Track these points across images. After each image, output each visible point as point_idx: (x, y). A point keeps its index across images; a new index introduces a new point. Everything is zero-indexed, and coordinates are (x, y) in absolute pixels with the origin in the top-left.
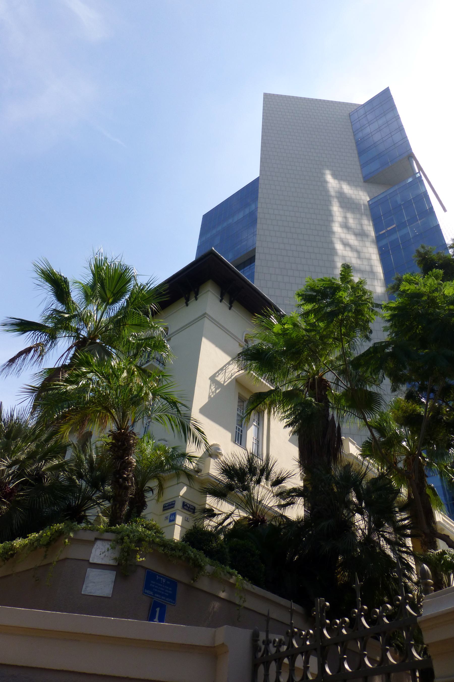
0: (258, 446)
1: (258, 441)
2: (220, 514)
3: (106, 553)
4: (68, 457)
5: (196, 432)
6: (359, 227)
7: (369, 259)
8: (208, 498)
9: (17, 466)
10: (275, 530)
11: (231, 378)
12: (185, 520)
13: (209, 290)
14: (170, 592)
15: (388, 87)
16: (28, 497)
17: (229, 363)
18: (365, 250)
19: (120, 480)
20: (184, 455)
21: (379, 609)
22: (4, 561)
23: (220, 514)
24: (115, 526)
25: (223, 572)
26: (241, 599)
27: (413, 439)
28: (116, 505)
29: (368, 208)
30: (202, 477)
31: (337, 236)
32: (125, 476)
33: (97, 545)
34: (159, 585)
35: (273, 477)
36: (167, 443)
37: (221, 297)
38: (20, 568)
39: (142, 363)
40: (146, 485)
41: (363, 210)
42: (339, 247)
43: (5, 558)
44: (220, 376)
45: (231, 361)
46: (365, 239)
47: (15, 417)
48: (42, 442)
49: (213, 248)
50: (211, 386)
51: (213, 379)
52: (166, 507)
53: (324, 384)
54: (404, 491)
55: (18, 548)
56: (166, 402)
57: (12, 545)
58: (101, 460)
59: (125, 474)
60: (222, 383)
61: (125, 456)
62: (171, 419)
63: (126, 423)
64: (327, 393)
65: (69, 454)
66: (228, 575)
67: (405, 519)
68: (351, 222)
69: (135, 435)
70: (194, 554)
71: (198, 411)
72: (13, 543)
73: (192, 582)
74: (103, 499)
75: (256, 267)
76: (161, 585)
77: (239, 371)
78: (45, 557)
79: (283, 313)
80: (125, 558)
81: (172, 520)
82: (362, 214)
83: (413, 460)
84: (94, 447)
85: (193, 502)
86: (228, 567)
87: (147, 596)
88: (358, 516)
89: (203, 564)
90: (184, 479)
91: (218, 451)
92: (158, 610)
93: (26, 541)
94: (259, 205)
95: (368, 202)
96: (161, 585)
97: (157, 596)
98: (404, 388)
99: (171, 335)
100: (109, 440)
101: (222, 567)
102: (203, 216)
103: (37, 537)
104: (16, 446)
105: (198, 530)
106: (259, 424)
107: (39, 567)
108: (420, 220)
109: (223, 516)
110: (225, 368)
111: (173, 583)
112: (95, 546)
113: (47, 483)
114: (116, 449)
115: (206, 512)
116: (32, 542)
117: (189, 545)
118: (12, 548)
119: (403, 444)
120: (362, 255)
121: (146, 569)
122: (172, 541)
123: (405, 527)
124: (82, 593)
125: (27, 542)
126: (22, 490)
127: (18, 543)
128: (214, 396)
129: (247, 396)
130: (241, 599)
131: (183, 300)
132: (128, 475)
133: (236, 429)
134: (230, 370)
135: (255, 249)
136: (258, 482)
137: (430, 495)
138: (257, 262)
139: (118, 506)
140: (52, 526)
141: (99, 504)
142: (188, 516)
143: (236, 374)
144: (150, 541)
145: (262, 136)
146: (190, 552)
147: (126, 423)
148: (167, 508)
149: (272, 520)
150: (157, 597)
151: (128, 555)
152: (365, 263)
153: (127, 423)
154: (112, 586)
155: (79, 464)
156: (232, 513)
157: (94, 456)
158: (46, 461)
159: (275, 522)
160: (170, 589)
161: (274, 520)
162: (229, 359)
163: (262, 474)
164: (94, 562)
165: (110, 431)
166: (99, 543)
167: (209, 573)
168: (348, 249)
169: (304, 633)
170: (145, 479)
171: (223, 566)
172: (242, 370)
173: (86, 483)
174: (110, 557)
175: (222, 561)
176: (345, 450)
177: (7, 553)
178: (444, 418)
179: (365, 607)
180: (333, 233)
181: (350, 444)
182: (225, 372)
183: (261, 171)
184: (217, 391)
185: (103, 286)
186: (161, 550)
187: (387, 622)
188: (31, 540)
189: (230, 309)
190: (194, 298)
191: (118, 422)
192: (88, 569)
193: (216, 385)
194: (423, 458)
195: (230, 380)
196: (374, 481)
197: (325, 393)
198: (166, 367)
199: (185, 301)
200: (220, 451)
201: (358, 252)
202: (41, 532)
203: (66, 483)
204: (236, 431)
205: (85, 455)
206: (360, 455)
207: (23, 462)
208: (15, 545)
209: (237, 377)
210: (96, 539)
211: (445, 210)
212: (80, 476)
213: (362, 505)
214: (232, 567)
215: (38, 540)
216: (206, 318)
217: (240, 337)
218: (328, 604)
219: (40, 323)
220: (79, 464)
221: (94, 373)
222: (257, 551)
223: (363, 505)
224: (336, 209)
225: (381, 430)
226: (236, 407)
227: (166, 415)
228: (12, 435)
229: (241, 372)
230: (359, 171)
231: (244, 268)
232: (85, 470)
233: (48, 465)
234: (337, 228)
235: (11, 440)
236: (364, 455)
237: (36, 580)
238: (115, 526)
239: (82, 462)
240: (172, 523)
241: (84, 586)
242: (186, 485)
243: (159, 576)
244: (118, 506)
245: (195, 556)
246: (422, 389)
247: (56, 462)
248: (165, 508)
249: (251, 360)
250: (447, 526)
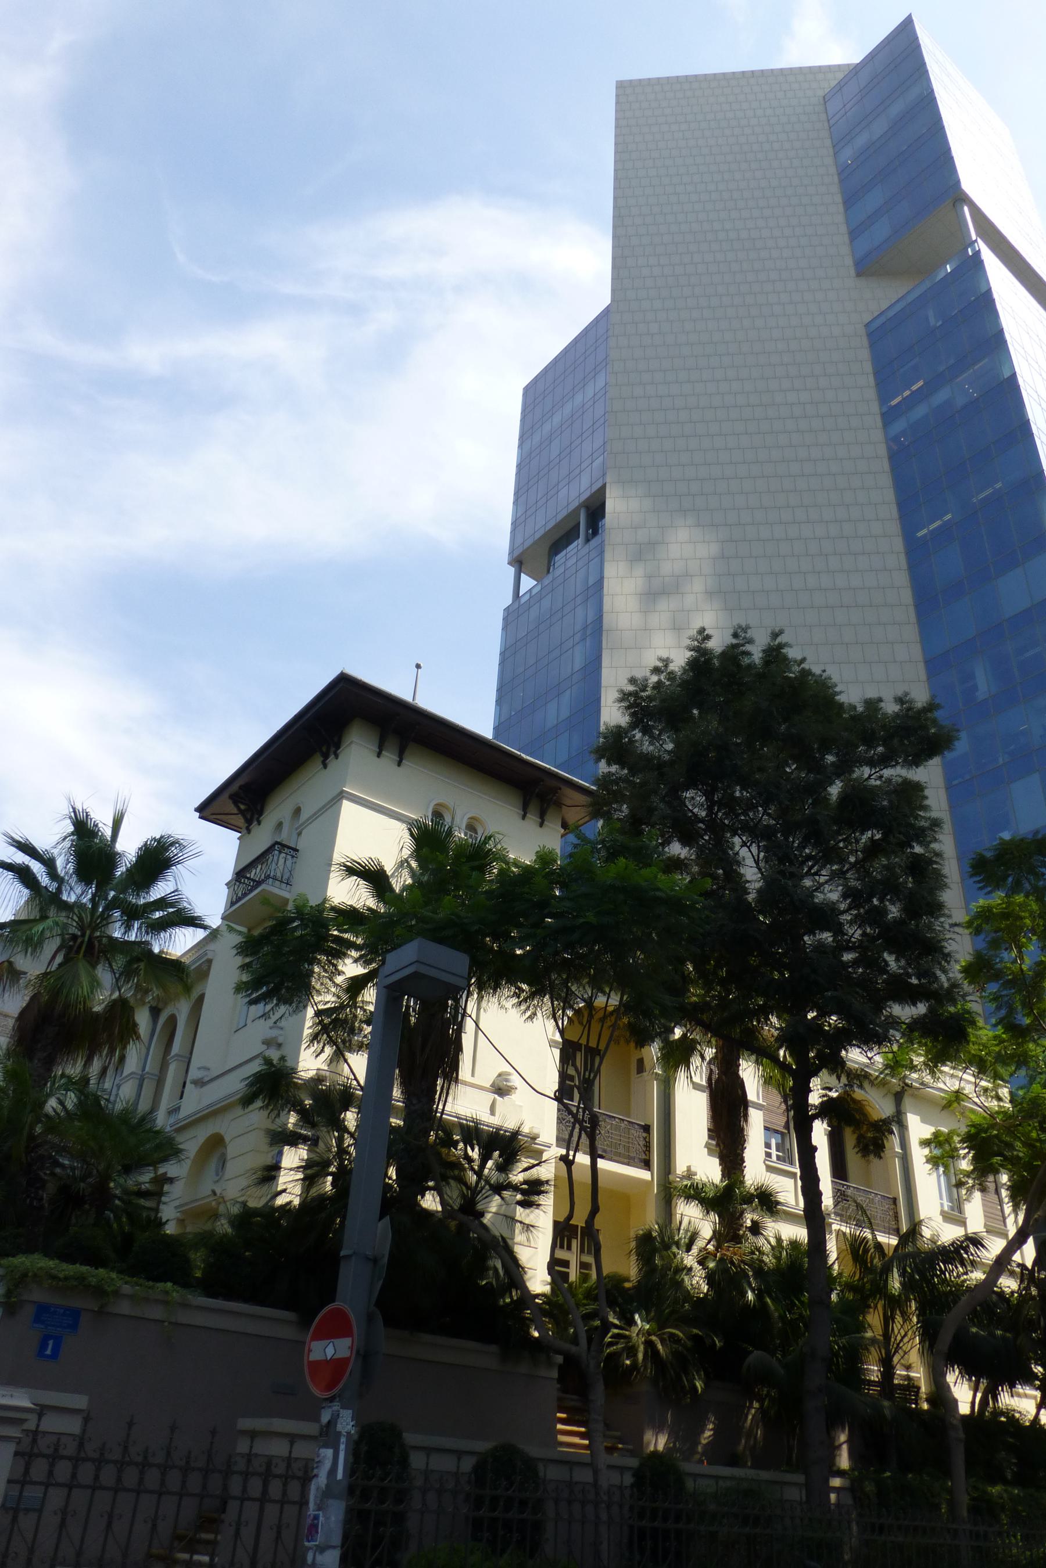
15: (910, 16)
36: (281, 1032)
37: (379, 748)
92: (51, 1342)
102: (527, 390)
110: (396, 874)
121: (34, 1302)
131: (318, 759)
145: (615, 198)
183: (613, 291)
199: (322, 759)
230: (845, 250)
231: (567, 546)
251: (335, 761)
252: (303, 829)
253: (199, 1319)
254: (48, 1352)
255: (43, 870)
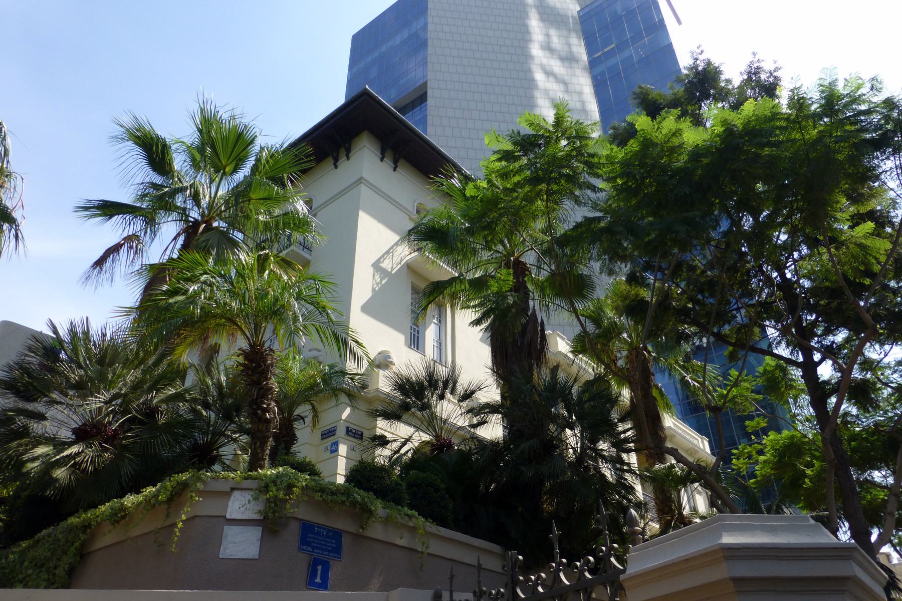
0: (440, 349)
1: (440, 344)
2: (395, 440)
3: (248, 506)
4: (189, 382)
5: (353, 344)
6: (566, 49)
7: (580, 93)
8: (378, 422)
9: (119, 401)
10: (464, 456)
11: (400, 263)
12: (351, 449)
13: (365, 145)
14: (333, 545)
16: (139, 439)
17: (396, 244)
18: (575, 80)
19: (259, 411)
20: (343, 373)
21: (580, 562)
22: (113, 524)
23: (395, 440)
24: (257, 470)
25: (400, 514)
26: (423, 545)
27: (636, 330)
28: (255, 444)
29: (578, 22)
30: (369, 394)
31: (537, 61)
32: (265, 406)
33: (235, 497)
34: (319, 538)
35: (460, 389)
36: (320, 353)
38: (136, 531)
39: (279, 249)
40: (295, 413)
41: (571, 25)
42: (539, 76)
43: (114, 520)
44: (386, 262)
45: (399, 241)
46: (575, 65)
47: (108, 338)
48: (149, 367)
49: (367, 87)
50: (374, 275)
51: (376, 266)
52: (324, 434)
53: (522, 268)
54: (626, 394)
55: (130, 507)
56: (312, 307)
57: (122, 504)
58: (232, 383)
59: (265, 404)
60: (390, 270)
61: (262, 380)
62: (319, 329)
63: (260, 337)
64: (526, 279)
65: (191, 379)
66: (406, 518)
67: (628, 430)
68: (556, 42)
69: (274, 353)
70: (361, 496)
71: (360, 309)
72: (122, 501)
73: (361, 530)
74: (241, 433)
75: (428, 108)
76: (322, 538)
77: (411, 254)
78: (168, 516)
79: (465, 172)
80: (272, 510)
81: (334, 450)
82: (569, 30)
83: (637, 356)
84: (222, 368)
85: (359, 426)
86: (406, 509)
87: (304, 553)
88: (568, 432)
89: (374, 508)
90: (343, 398)
91: (388, 360)
92: (319, 568)
93: (140, 498)
94: (430, 20)
95: (579, 12)
96: (322, 538)
97: (318, 551)
98: (625, 269)
99: (316, 209)
100: (241, 359)
101: (398, 509)
102: (358, 39)
103: (154, 493)
104: (114, 374)
105: (365, 466)
106: (440, 322)
107: (161, 529)
108: (647, 37)
109: (398, 444)
110: (392, 250)
111: (337, 535)
112: (232, 498)
113: (162, 420)
114: (250, 372)
115: (376, 439)
116: (148, 499)
117: (354, 487)
118: (123, 508)
119: (624, 335)
120: (571, 87)
121: (301, 520)
122: (334, 484)
123: (626, 441)
124: (220, 557)
125: (141, 499)
126: (129, 430)
127: (130, 500)
128: (379, 289)
129: (422, 286)
130: (423, 545)
131: (330, 160)
132: (268, 405)
133: (411, 330)
134: (398, 253)
135: (427, 82)
136: (442, 397)
137: (657, 398)
138: (430, 101)
139: (258, 445)
140: (173, 477)
141: (235, 440)
142: (354, 444)
143: (409, 257)
144: (302, 486)
146: (355, 495)
147: (260, 337)
148: (326, 436)
149: (460, 444)
150: (318, 553)
151: (276, 505)
152: (575, 98)
153: (262, 338)
154: (258, 544)
155: (205, 392)
156: (410, 438)
157: (223, 378)
158: (158, 391)
159: (465, 445)
160: (333, 541)
161: (463, 443)
162: (396, 238)
163: (445, 386)
164: (233, 518)
165: (239, 349)
166: (236, 494)
167: (382, 518)
168: (551, 79)
169: (493, 592)
170: (293, 405)
171: (399, 507)
172: (414, 252)
173: (216, 415)
174: (253, 510)
175: (398, 502)
176: (551, 348)
177: (116, 515)
178: (674, 304)
179: (564, 560)
180: (531, 57)
181: (559, 340)
182: (393, 256)
184: (383, 282)
185: (213, 147)
186: (317, 496)
187: (590, 577)
188: (146, 496)
189: (395, 170)
190: (345, 158)
191: (249, 336)
192: (225, 527)
193: (380, 274)
194: (649, 352)
195: (400, 266)
196: (589, 384)
197: (523, 280)
198: (313, 253)
200: (391, 360)
201: (565, 83)
202: (159, 484)
203: (190, 417)
204: (411, 333)
205: (212, 379)
206: (571, 352)
207: (125, 395)
208: (126, 503)
209: (408, 262)
210: (233, 489)
211: (679, 21)
212: (207, 406)
213: (572, 419)
214: (412, 507)
215: (156, 496)
216: (362, 184)
217: (410, 208)
218: (521, 557)
219: (131, 204)
220: (205, 392)
221: (208, 274)
222: (442, 485)
223: (574, 417)
224: (534, 23)
225: (596, 319)
226: (410, 301)
227: (312, 325)
228: (107, 361)
229: (413, 255)
231: (413, 110)
232: (213, 397)
233: (161, 396)
234: (536, 51)
235: (106, 367)
236: (575, 352)
237: (159, 546)
238: (257, 470)
239: (208, 387)
240: (335, 454)
241: (222, 548)
242: (349, 406)
243: (318, 527)
244: (258, 445)
245: (363, 500)
246: (648, 267)
247: (172, 391)
248: (324, 437)
249: (425, 240)
250: (679, 431)
251: (347, 163)
252: (318, 211)
253: (436, 548)
254: (318, 580)
255: (195, 135)
